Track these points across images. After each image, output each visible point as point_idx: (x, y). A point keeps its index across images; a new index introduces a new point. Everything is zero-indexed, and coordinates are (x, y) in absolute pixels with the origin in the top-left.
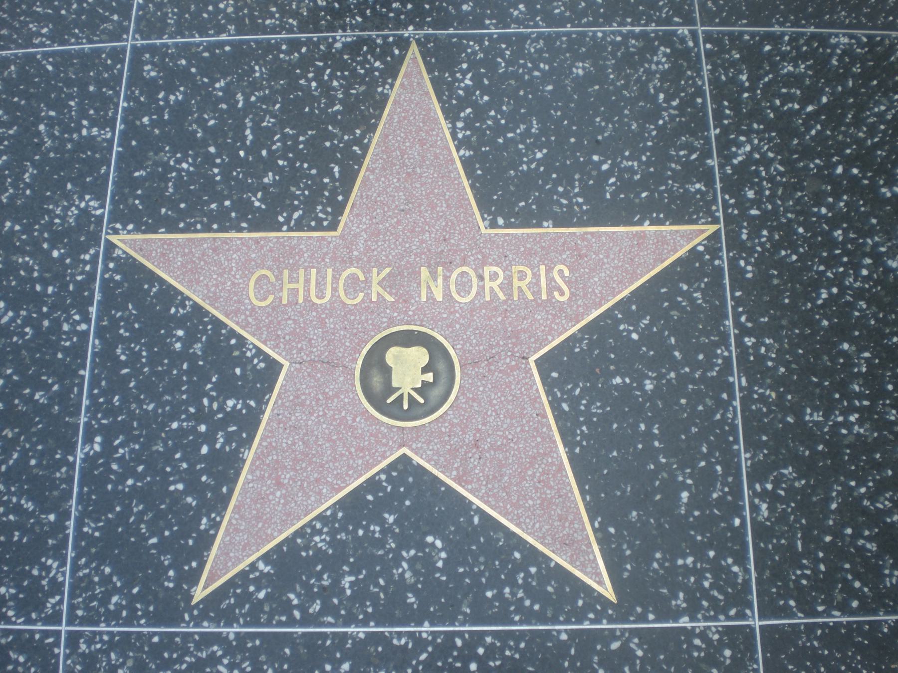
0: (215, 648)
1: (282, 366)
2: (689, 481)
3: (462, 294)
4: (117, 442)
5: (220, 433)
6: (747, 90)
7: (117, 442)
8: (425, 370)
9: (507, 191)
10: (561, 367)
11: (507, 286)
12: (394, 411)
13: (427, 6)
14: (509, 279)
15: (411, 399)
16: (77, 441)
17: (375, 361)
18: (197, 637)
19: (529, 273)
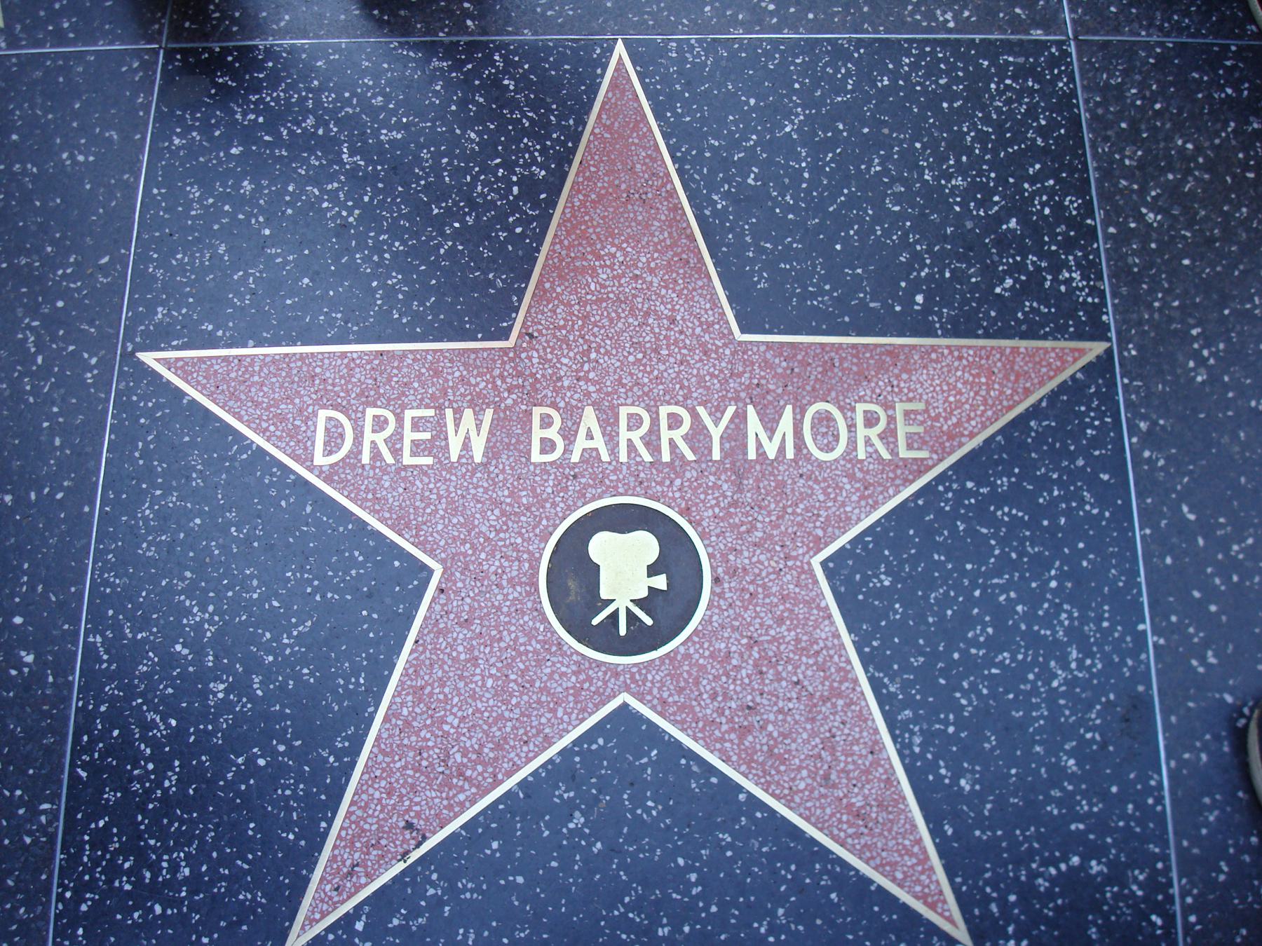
1: (431, 572)
2: (654, 813)
3: (594, 454)
6: (44, 204)
8: (653, 570)
10: (394, 583)
11: (652, 441)
12: (605, 638)
14: (655, 429)
15: (631, 616)
16: (1156, 663)
17: (574, 573)
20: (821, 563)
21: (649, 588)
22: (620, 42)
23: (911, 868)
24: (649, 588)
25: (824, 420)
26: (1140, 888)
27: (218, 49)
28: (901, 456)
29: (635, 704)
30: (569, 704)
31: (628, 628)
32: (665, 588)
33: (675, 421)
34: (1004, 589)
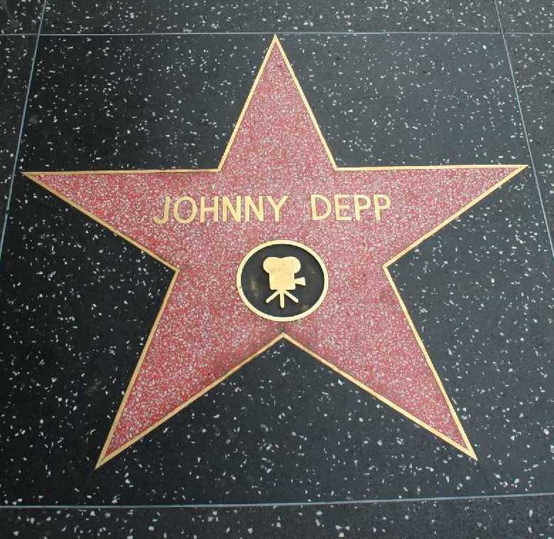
0: (108, 115)
8: (297, 276)
9: (365, 131)
10: (161, 276)
12: (274, 308)
17: (256, 277)
18: (111, 38)
19: (369, 201)
21: (296, 285)
22: (275, 36)
24: (296, 285)
25: (189, 206)
27: (24, 37)
28: (335, 196)
29: (287, 337)
30: (248, 334)
31: (270, 302)
32: (304, 284)
34: (143, 276)
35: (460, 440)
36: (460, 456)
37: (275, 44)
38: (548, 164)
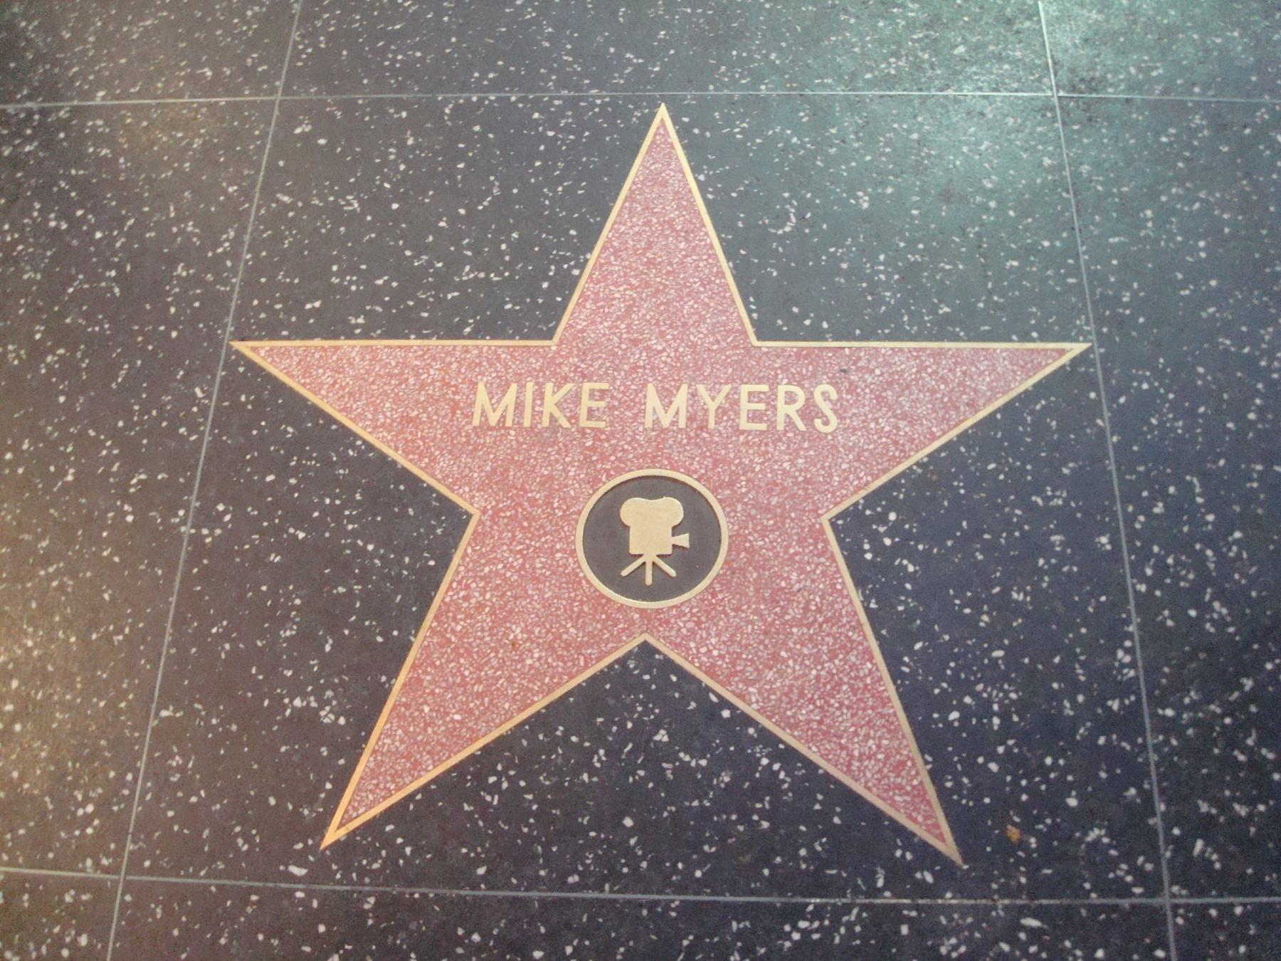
4: (1207, 598)
5: (159, 916)
7: (1207, 598)
8: (676, 530)
10: (852, 527)
12: (633, 587)
13: (559, 299)
17: (607, 539)
20: (830, 520)
21: (674, 546)
23: (873, 753)
24: (674, 546)
26: (63, 382)
33: (791, 399)
35: (341, 825)
36: (781, 746)
37: (662, 120)
38: (1205, 309)
